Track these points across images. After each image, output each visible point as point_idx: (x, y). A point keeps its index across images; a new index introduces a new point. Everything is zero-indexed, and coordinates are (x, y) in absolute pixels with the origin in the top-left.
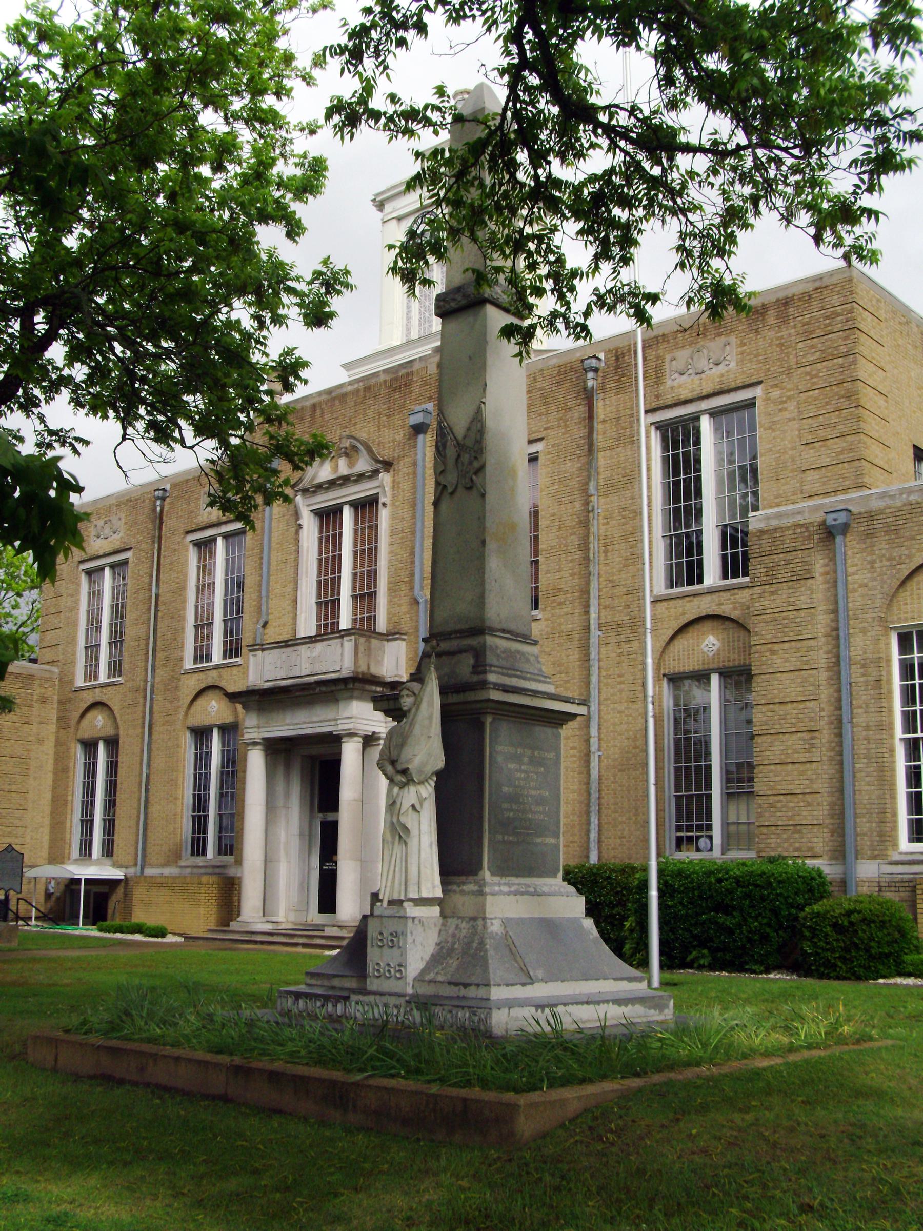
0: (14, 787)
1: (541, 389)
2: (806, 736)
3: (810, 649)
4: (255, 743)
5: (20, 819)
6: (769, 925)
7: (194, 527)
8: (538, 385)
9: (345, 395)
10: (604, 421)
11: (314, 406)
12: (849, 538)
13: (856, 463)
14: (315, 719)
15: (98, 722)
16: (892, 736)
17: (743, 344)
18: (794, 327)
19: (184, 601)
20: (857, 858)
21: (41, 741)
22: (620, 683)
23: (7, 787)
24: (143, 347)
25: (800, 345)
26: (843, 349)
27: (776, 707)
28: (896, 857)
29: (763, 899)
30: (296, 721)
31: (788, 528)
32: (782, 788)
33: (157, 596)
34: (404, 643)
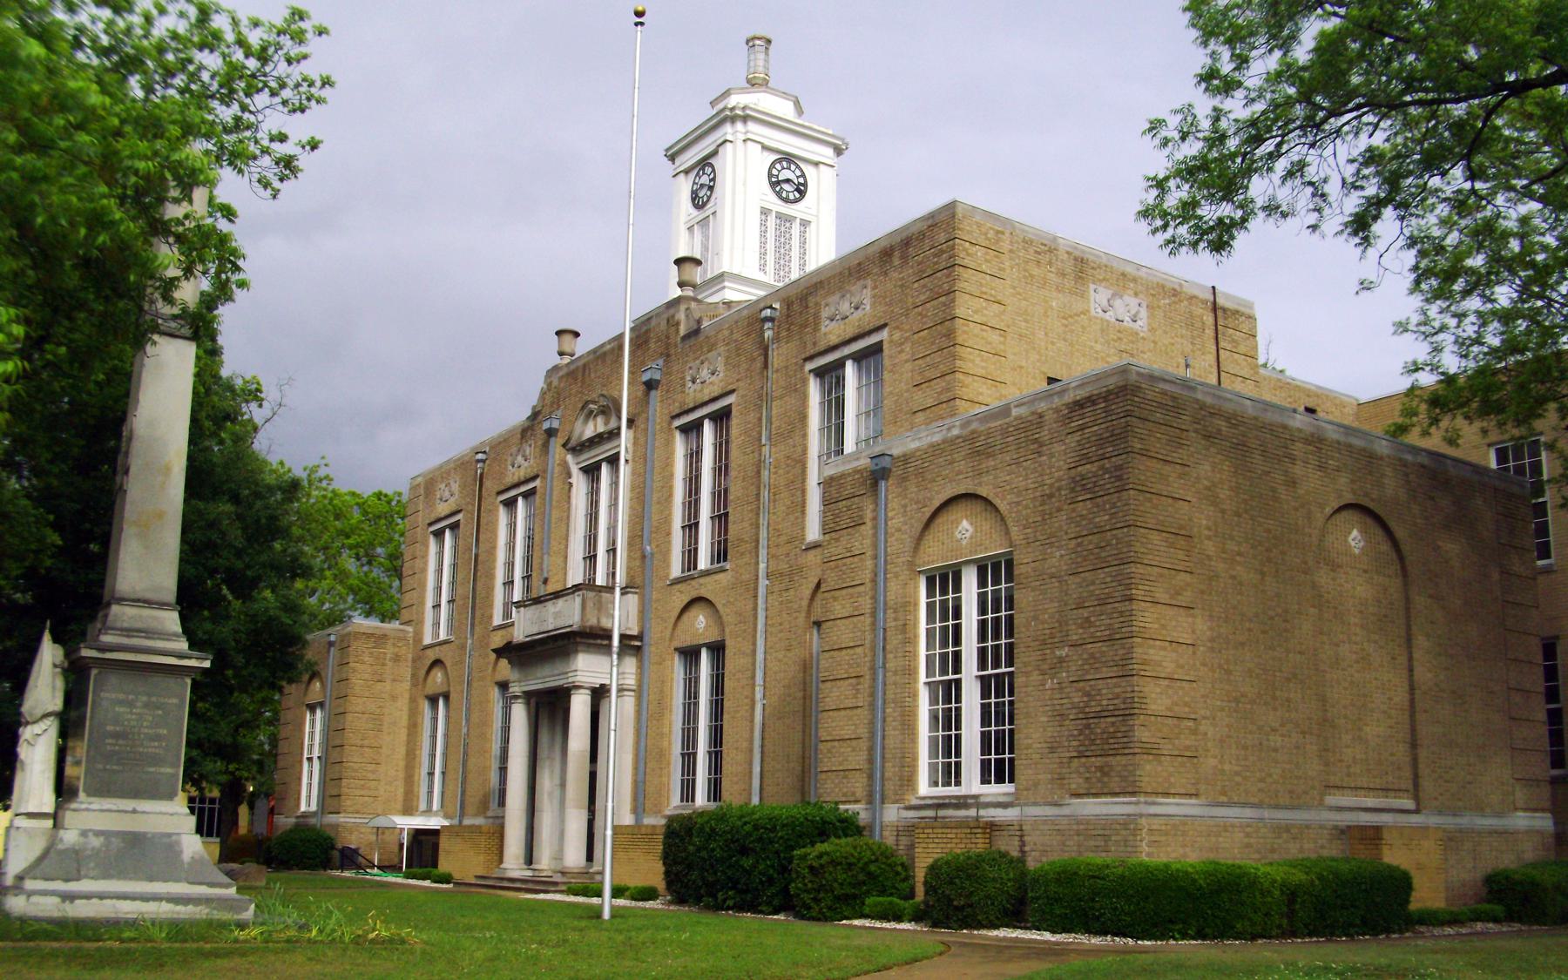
0: (366, 742)
1: (736, 341)
2: (853, 681)
3: (859, 595)
4: (516, 697)
5: (373, 772)
6: (773, 866)
7: (503, 488)
8: (735, 336)
9: (605, 354)
10: (777, 371)
11: (585, 366)
12: (891, 482)
13: (952, 403)
14: (556, 672)
15: (700, 625)
16: (916, 680)
17: (875, 287)
18: (912, 267)
19: (494, 561)
20: (883, 803)
21: (394, 698)
22: (781, 631)
23: (359, 743)
24: (1517, 130)
25: (916, 285)
26: (946, 287)
27: (835, 654)
28: (914, 802)
29: (771, 842)
30: (556, 672)
31: (849, 474)
32: (837, 733)
33: (477, 556)
34: (636, 596)
